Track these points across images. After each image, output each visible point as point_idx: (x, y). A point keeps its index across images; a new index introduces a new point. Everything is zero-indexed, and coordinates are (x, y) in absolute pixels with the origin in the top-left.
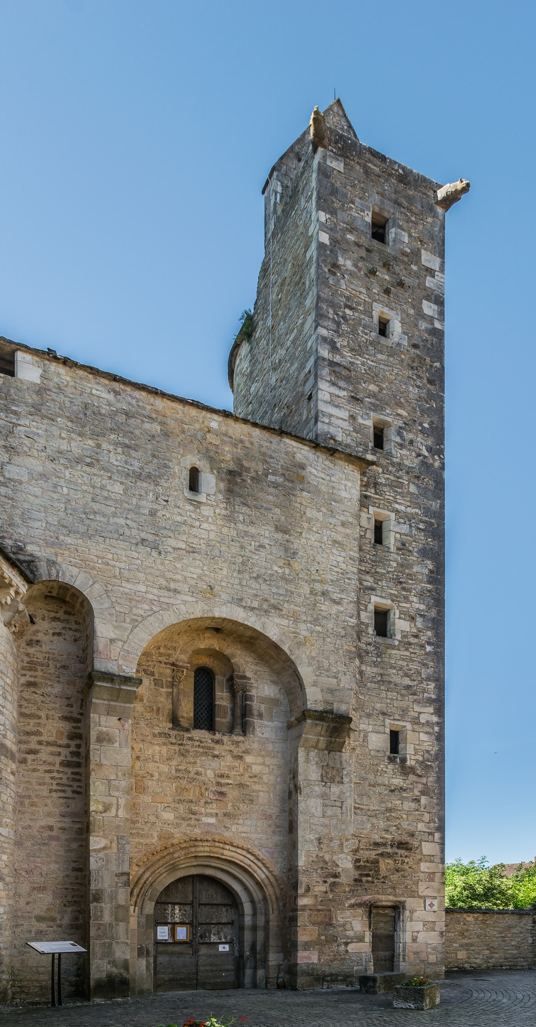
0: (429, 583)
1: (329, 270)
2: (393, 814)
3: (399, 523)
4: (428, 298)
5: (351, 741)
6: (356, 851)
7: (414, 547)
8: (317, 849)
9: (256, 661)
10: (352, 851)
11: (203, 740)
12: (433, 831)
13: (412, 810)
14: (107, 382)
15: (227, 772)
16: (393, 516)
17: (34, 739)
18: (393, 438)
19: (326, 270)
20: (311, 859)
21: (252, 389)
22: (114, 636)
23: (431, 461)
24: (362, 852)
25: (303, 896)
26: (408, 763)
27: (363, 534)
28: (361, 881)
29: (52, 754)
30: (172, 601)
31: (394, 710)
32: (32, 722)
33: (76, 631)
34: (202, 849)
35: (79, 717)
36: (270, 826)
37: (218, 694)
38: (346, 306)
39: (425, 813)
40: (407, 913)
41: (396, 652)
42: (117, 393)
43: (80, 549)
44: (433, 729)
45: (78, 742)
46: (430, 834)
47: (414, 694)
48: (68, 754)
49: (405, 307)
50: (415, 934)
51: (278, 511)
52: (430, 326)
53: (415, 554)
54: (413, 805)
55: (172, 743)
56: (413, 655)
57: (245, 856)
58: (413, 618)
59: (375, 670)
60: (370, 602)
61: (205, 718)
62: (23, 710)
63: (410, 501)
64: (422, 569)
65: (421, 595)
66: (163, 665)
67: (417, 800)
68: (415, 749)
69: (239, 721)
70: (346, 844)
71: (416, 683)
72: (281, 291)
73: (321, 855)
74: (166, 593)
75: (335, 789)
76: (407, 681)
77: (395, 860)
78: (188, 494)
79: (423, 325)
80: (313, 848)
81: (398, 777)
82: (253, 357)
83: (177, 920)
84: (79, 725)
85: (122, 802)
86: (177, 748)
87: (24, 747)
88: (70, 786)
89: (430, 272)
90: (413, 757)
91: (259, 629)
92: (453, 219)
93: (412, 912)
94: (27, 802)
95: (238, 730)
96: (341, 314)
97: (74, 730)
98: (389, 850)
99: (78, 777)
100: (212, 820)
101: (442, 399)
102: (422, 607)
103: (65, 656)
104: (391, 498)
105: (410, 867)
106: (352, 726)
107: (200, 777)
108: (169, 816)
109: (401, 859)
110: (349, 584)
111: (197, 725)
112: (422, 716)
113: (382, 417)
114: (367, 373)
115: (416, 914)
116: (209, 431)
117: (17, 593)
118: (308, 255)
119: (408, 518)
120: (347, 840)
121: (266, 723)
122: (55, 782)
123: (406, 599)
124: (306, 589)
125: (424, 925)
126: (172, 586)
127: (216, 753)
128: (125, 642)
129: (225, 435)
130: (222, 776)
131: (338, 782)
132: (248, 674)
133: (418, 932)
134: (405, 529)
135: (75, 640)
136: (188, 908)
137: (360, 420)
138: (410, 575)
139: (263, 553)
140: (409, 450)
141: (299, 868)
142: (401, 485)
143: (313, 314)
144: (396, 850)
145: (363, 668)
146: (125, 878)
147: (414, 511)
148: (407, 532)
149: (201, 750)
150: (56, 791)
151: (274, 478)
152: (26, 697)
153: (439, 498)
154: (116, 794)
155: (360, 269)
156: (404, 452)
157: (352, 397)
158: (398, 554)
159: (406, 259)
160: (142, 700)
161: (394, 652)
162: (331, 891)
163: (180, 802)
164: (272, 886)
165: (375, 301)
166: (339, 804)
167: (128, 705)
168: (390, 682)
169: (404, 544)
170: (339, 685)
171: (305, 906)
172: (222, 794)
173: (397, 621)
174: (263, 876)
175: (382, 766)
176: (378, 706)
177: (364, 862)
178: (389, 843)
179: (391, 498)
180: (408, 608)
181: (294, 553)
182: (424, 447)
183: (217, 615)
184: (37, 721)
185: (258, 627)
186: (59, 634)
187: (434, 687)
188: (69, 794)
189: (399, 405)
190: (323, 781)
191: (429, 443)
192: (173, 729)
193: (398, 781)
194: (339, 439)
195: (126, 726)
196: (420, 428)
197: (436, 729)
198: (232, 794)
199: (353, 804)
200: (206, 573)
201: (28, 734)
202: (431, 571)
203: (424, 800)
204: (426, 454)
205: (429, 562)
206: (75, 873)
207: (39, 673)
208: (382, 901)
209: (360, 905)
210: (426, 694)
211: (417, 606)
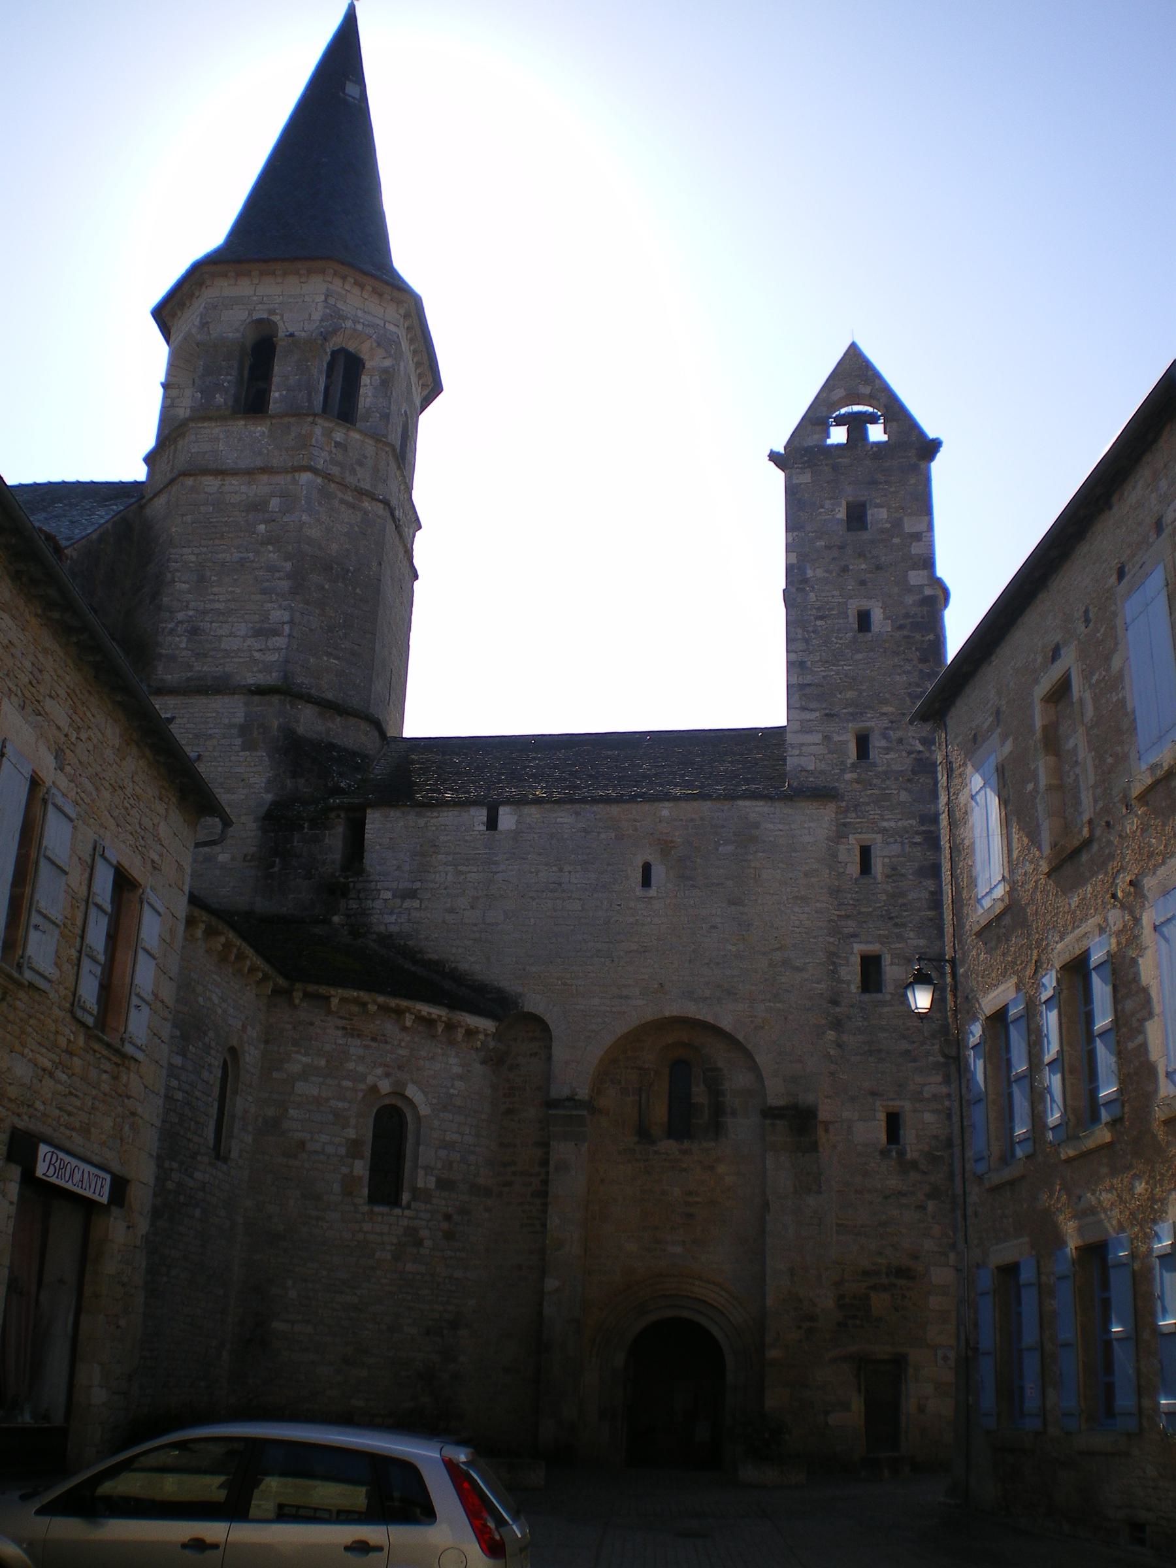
0: (930, 909)
1: (797, 589)
14: (569, 806)
26: (909, 1156)
42: (577, 814)
47: (914, 1061)
51: (729, 883)
52: (917, 597)
53: (910, 877)
60: (852, 953)
67: (921, 1207)
71: (915, 1045)
76: (905, 1045)
78: (639, 892)
100: (678, 1249)
102: (922, 942)
106: (823, 1115)
111: (670, 1135)
113: (862, 725)
117: (486, 1035)
134: (895, 848)
137: (836, 738)
138: (904, 905)
145: (845, 1038)
156: (892, 755)
157: (826, 715)
161: (886, 1010)
165: (851, 598)
168: (880, 1051)
169: (894, 869)
173: (888, 968)
183: (667, 1014)
186: (536, 1054)
191: (924, 734)
203: (931, 1205)
204: (921, 748)
210: (931, 1058)
211: (915, 942)
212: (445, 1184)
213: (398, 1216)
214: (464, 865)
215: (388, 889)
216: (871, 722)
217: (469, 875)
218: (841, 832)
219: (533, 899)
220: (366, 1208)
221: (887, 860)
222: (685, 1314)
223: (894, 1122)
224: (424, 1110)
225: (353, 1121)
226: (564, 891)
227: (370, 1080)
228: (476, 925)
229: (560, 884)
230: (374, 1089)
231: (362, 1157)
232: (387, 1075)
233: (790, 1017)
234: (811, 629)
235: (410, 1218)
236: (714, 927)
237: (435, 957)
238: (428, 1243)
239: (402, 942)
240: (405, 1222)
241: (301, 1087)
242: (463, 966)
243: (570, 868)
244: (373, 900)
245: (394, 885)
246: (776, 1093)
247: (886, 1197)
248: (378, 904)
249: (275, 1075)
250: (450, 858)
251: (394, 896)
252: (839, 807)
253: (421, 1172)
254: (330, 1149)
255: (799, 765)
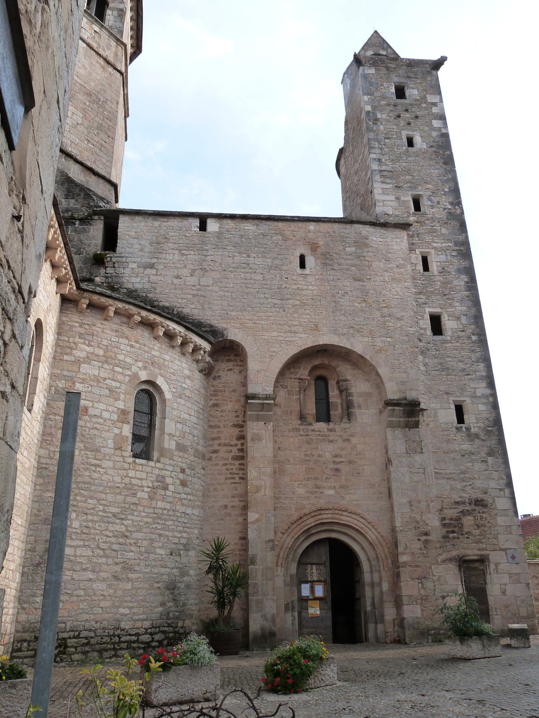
1: (373, 123)
2: (466, 475)
3: (438, 255)
4: (435, 118)
5: (423, 419)
6: (441, 510)
7: (452, 269)
8: (409, 511)
9: (353, 367)
10: (438, 511)
11: (321, 430)
12: (503, 487)
13: (482, 470)
15: (339, 453)
16: (433, 251)
17: (217, 442)
18: (426, 203)
19: (371, 123)
20: (405, 520)
21: (347, 184)
22: (259, 368)
23: (454, 211)
24: (445, 511)
25: (403, 553)
26: (472, 430)
27: (414, 268)
28: (448, 537)
29: (227, 452)
30: (293, 339)
31: (454, 389)
32: (215, 430)
33: (240, 366)
34: (326, 516)
35: (243, 423)
36: (374, 493)
37: (331, 393)
38: (385, 138)
39: (494, 472)
40: (492, 566)
41: (450, 345)
42: (257, 225)
43: (239, 317)
44: (488, 400)
45: (242, 441)
46: (501, 490)
48: (236, 451)
49: (421, 128)
50: (503, 586)
53: (453, 273)
54: (483, 466)
55: (301, 435)
56: (463, 345)
57: (358, 520)
58: (458, 318)
59: (436, 361)
61: (324, 414)
62: (211, 423)
63: (444, 239)
64: (461, 281)
65: (462, 300)
66: (293, 380)
68: (476, 418)
69: (346, 412)
70: (432, 505)
71: (468, 365)
72: (353, 133)
73: (413, 516)
74: (290, 335)
75: (418, 458)
76: (461, 365)
77: (475, 517)
78: (299, 271)
79: (434, 134)
80: (407, 510)
81: (467, 443)
82: (346, 166)
83: (315, 579)
84: (243, 429)
85: (268, 484)
86: (304, 438)
87: (210, 449)
88: (238, 474)
89: (435, 104)
90: (475, 425)
91: (349, 347)
92: (442, 73)
93: (497, 565)
94: (212, 488)
95: (345, 420)
96: (382, 143)
97: (239, 433)
98: (468, 508)
99: (242, 467)
100: (332, 492)
101: (455, 172)
103: (234, 384)
104: (430, 240)
105: (488, 522)
106: (422, 406)
107: (321, 459)
108: (301, 491)
109: (479, 515)
110: (407, 305)
111: (318, 420)
112: (477, 391)
113: (416, 193)
114: (403, 171)
115: (500, 567)
116: (309, 232)
117: (205, 352)
118: (362, 116)
119: (444, 250)
120: (432, 501)
121: (364, 411)
122: (228, 472)
123: (451, 305)
124: (378, 314)
125: (510, 578)
126: (293, 329)
127: (331, 438)
128: (266, 371)
129: (318, 232)
130: (336, 456)
131: (419, 453)
132: (349, 377)
133: (505, 584)
134: (443, 258)
135: (240, 372)
136: (322, 568)
139: (347, 297)
140: (438, 207)
141: (397, 528)
142: (435, 231)
143: (367, 147)
144: (475, 508)
146: (271, 544)
147: (447, 245)
148: (445, 259)
149: (321, 438)
150: (229, 478)
151: (350, 249)
152: (212, 414)
153: (464, 233)
154: (264, 478)
155: (391, 117)
157: (396, 187)
158: (440, 276)
159: (418, 103)
160: (280, 406)
162: (425, 547)
163: (308, 479)
164: (382, 546)
165: (403, 130)
166: (422, 471)
167: (269, 413)
168: (448, 369)
170: (408, 378)
171: (405, 562)
172: (337, 470)
173: (447, 322)
174: (374, 537)
175: (451, 435)
176: (442, 388)
177: (449, 520)
178: (467, 501)
179: (430, 240)
180: (454, 311)
181: (367, 293)
182: (448, 204)
184: (218, 430)
185: (348, 346)
186: (231, 370)
187: (484, 366)
188: (237, 480)
189: (426, 183)
190: (407, 453)
191: (451, 200)
192: (301, 424)
193: (466, 446)
194: (390, 213)
195: (269, 427)
196: (443, 193)
197: (491, 399)
198: (344, 468)
199: (433, 470)
200: (313, 317)
201: (213, 439)
202: (467, 283)
203: (490, 460)
204: (450, 207)
205: (464, 276)
206: (242, 541)
207: (220, 397)
208: (468, 556)
209: (450, 560)
210: (478, 373)
211: (460, 308)
212: (180, 447)
213: (152, 467)
214: (185, 250)
215: (134, 262)
216: (419, 191)
217: (189, 256)
218: (412, 248)
219: (231, 272)
220: (131, 460)
221: (439, 264)
222: (334, 535)
223: (459, 410)
224: (168, 395)
225: (122, 397)
226: (251, 268)
227: (134, 369)
228: (194, 286)
229: (248, 264)
230: (135, 376)
231: (128, 423)
232: (145, 368)
233: (397, 346)
234: (382, 143)
235: (160, 469)
236: (347, 293)
237: (167, 304)
238: (171, 488)
239: (144, 295)
240: (157, 472)
241: (85, 368)
242: (186, 311)
243: (255, 255)
244: (124, 268)
245: (139, 260)
246: (392, 392)
247: (463, 456)
248: (127, 271)
249: (66, 357)
250: (176, 246)
251: (138, 267)
252: (408, 234)
253: (166, 437)
254: (106, 415)
255: (383, 211)
